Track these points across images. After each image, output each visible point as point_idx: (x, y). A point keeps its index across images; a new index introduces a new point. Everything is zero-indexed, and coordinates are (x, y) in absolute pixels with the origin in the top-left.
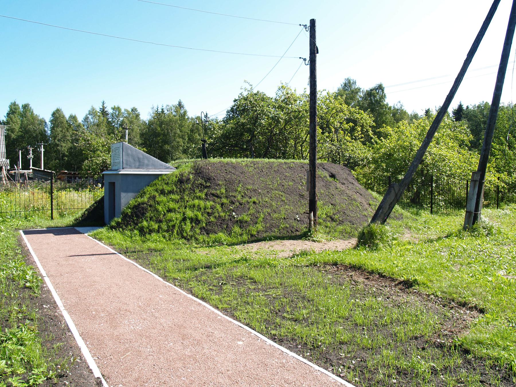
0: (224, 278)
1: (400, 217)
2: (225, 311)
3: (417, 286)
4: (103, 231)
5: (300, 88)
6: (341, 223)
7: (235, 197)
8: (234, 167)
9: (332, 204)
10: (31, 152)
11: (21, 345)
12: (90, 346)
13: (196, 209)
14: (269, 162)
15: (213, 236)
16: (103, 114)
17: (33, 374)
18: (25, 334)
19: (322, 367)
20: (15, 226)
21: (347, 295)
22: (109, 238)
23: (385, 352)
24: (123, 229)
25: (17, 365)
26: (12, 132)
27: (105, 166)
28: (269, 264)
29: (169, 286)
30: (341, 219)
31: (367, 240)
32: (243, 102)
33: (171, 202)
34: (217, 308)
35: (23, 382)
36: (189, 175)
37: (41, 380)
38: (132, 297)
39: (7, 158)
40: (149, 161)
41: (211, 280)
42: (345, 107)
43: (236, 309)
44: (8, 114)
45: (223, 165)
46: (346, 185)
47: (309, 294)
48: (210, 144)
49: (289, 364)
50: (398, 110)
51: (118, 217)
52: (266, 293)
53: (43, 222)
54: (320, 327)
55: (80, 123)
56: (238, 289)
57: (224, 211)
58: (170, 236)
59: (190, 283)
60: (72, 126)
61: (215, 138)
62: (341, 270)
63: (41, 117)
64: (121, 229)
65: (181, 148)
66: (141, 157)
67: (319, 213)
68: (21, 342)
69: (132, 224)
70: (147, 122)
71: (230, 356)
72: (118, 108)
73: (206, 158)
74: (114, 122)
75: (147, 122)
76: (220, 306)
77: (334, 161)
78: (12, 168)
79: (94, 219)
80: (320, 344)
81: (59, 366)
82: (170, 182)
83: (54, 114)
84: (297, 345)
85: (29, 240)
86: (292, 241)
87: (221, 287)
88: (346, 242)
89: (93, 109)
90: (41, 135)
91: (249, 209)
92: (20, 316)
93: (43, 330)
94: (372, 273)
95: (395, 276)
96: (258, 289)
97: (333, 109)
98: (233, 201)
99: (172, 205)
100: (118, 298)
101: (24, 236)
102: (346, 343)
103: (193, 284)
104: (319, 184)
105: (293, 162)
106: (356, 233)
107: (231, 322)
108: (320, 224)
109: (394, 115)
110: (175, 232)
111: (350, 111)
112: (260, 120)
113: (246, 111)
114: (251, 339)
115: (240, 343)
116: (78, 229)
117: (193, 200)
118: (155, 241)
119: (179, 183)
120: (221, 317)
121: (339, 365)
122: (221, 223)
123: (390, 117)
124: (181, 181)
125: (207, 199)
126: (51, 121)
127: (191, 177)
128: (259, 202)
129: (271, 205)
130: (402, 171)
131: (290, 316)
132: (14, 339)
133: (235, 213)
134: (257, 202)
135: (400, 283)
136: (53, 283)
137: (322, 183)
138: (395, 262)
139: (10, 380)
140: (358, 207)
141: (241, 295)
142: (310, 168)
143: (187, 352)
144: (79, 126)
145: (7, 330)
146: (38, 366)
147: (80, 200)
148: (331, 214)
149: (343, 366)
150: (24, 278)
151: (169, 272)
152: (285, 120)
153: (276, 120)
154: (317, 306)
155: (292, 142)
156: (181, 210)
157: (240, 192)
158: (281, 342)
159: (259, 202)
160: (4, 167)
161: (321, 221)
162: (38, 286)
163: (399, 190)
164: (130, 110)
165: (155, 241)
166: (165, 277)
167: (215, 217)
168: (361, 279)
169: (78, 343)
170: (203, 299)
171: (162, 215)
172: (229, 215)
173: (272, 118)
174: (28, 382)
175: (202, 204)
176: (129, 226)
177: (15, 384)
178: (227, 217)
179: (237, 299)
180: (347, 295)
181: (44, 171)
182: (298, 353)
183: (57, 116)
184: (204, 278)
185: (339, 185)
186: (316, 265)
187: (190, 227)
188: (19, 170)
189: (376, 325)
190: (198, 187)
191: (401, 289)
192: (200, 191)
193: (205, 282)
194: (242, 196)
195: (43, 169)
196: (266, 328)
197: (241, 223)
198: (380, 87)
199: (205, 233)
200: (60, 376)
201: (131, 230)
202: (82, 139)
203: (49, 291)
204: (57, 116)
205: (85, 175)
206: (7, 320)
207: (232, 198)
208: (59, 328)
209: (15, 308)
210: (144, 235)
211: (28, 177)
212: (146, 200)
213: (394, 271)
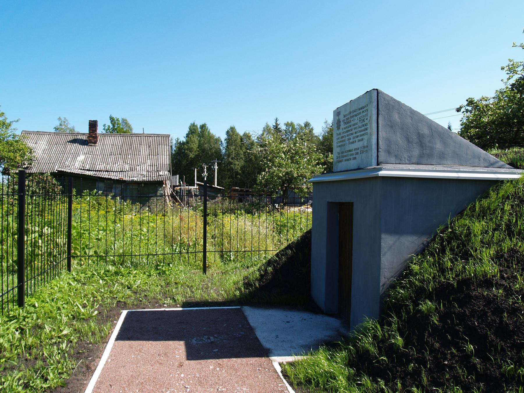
10: (205, 170)
40: (445, 144)
44: (188, 136)
55: (253, 141)
63: (217, 136)
70: (321, 138)
72: (292, 123)
75: (321, 138)
83: (228, 132)
89: (267, 126)
90: (216, 153)
144: (252, 144)
183: (231, 133)
204: (231, 133)
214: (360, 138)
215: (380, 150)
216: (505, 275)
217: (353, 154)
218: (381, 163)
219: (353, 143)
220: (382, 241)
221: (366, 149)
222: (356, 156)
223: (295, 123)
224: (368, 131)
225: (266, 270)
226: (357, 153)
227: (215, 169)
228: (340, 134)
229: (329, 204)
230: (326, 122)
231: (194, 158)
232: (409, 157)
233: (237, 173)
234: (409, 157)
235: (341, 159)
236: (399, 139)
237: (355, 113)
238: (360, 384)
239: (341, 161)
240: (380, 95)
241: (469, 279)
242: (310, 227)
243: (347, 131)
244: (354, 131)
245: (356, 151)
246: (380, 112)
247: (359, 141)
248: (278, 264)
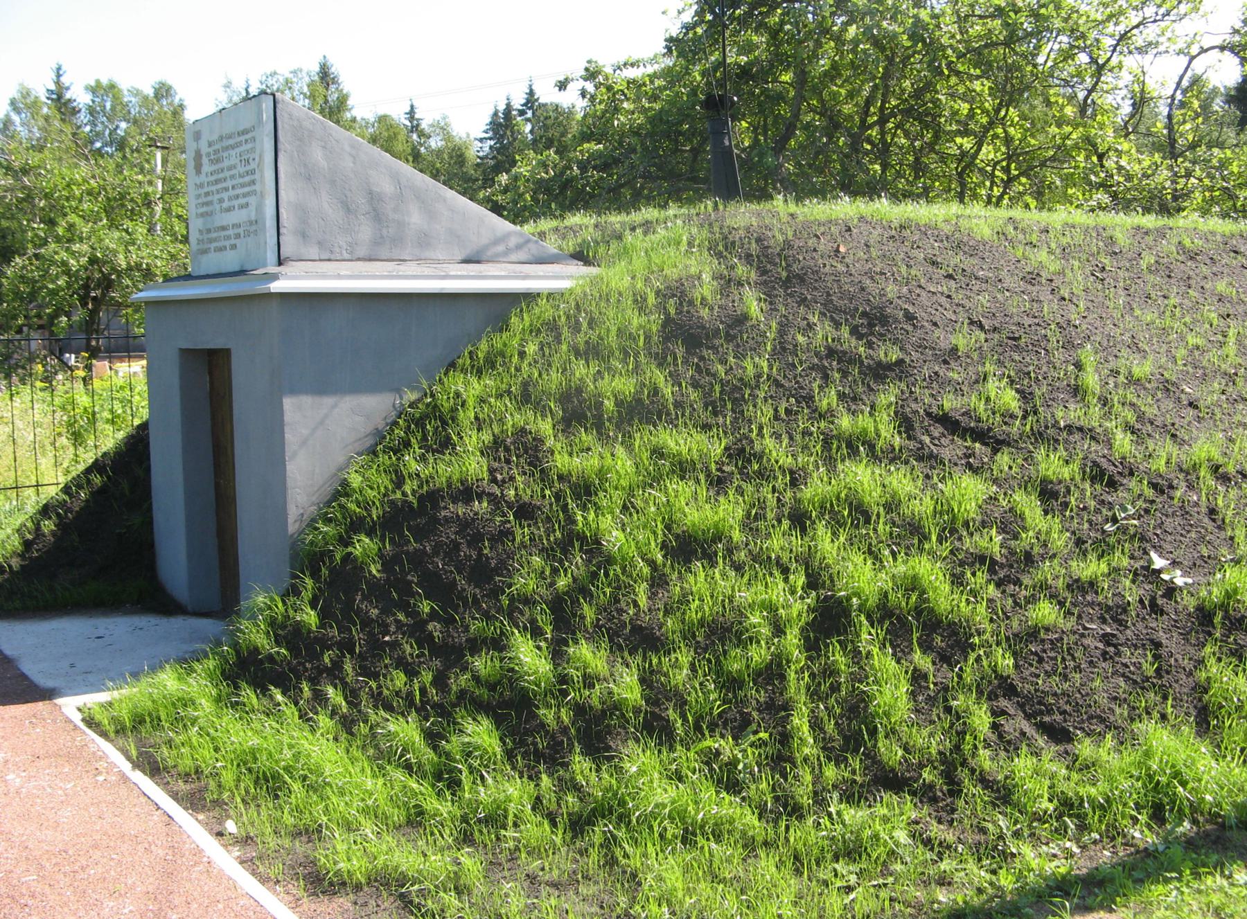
66: (386, 187)
72: (112, 86)
89: (26, 94)
99: (697, 509)
124: (685, 333)
164: (150, 92)
210: (554, 757)
214: (242, 201)
215: (282, 230)
216: (499, 477)
217: (229, 238)
218: (288, 259)
219: (229, 210)
220: (287, 429)
221: (254, 228)
222: (237, 242)
223: (124, 85)
224: (257, 187)
225: (38, 528)
226: (238, 236)
228: (201, 186)
229: (187, 354)
230: (227, 86)
232: (350, 244)
234: (350, 244)
235: (206, 246)
236: (326, 206)
237: (231, 142)
238: (237, 703)
239: (205, 252)
240: (279, 106)
241: (439, 490)
242: (144, 414)
243: (217, 182)
244: (229, 184)
245: (236, 231)
246: (280, 146)
247: (242, 207)
248: (69, 510)
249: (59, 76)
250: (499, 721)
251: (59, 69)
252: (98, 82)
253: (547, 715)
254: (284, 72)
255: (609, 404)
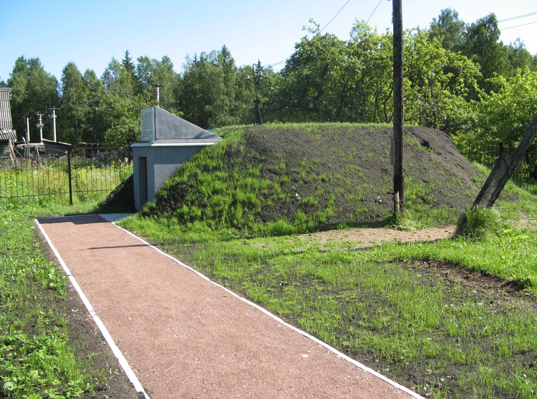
0: (285, 277)
1: (514, 198)
2: (286, 317)
3: (529, 288)
4: (133, 218)
5: (383, 27)
6: (436, 205)
7: (298, 173)
8: (297, 134)
9: (424, 181)
10: (41, 119)
11: (52, 354)
12: (129, 357)
13: (249, 189)
14: (341, 127)
15: (271, 225)
16: (127, 68)
17: (70, 386)
18: (55, 342)
19: (403, 385)
20: (28, 214)
21: (439, 299)
22: (141, 227)
23: (482, 369)
24: (158, 217)
25: (51, 375)
26: (18, 95)
27: (132, 137)
28: (341, 260)
29: (217, 287)
30: (436, 200)
31: (469, 227)
32: (307, 48)
33: (217, 182)
34: (277, 314)
35: (59, 395)
36: (238, 146)
37: (79, 392)
38: (173, 300)
39: (13, 129)
41: (269, 280)
42: (442, 51)
43: (300, 316)
45: (282, 132)
46: (443, 156)
47: (391, 296)
48: (266, 103)
49: (364, 380)
50: (516, 50)
51: (152, 201)
52: (337, 296)
53: (60, 208)
54: (403, 337)
55: (98, 81)
56: (303, 291)
57: (284, 192)
58: (217, 224)
59: (243, 284)
60: (89, 85)
61: (271, 96)
62: (434, 266)
64: (156, 217)
65: (227, 108)
67: (406, 193)
68: (51, 351)
69: (169, 209)
71: (293, 370)
73: (260, 123)
74: (141, 77)
75: (182, 76)
76: (281, 312)
77: (429, 124)
78: (20, 141)
79: (122, 203)
80: (402, 358)
81: (96, 379)
82: (215, 155)
83: (66, 71)
84: (374, 359)
85: (46, 231)
86: (371, 230)
87: (281, 288)
88: (442, 230)
89: (114, 62)
91: (316, 188)
92: (47, 321)
93: (73, 339)
94: (473, 270)
95: (502, 275)
96: (328, 291)
97: (426, 54)
98: (296, 178)
99: (218, 185)
100: (157, 301)
101: (40, 226)
102: (435, 357)
103: (246, 284)
104: (406, 155)
105: (374, 127)
106: (456, 219)
107: (293, 331)
108: (408, 207)
109: (510, 58)
110: (223, 218)
111: (449, 57)
112: (331, 71)
113: (312, 58)
114: (318, 351)
115: (305, 356)
116: (103, 216)
117: (245, 178)
118: (198, 231)
119: (226, 157)
120: (282, 324)
121: (423, 382)
122: (281, 207)
123: (504, 60)
124: (229, 154)
125: (262, 177)
126: (63, 80)
127: (242, 148)
128: (330, 180)
129: (345, 184)
130: (519, 136)
131: (367, 324)
132: (44, 347)
133: (299, 194)
134: (327, 180)
135: (508, 284)
136: (80, 283)
137: (411, 154)
138: (503, 257)
139: (46, 391)
140: (458, 184)
141: (306, 297)
142: (394, 132)
143: (242, 366)
144: (98, 84)
145: (35, 337)
146: (74, 378)
147: (103, 179)
148: (423, 194)
149: (429, 384)
150: (47, 278)
151: (216, 269)
152: (363, 69)
153: (351, 70)
154: (400, 313)
155: (372, 99)
156: (229, 191)
157: (304, 166)
158: (354, 354)
159: (330, 180)
160: (10, 141)
161: (409, 203)
162: (63, 286)
163: (512, 163)
165: (199, 231)
166: (212, 277)
167: (273, 200)
168: (459, 279)
169: (114, 353)
170: (259, 303)
171: (206, 199)
172: (291, 197)
173: (347, 69)
174: (64, 394)
175: (256, 183)
176: (166, 213)
177: (52, 396)
178: (288, 200)
179: (301, 304)
180: (439, 299)
181: (57, 144)
182: (376, 368)
183: (70, 72)
184: (260, 277)
185: (433, 156)
186: (402, 261)
187: (241, 213)
188: (27, 143)
189: (474, 336)
190: (250, 161)
191: (508, 292)
192: (253, 166)
193: (261, 282)
194: (308, 172)
195: (55, 141)
196: (336, 338)
197: (306, 207)
198: (491, 20)
199: (260, 220)
200: (99, 389)
201: (169, 218)
202: (104, 102)
203: (76, 293)
204: (70, 72)
205: (108, 147)
206: (34, 326)
207: (294, 174)
208: (92, 336)
209: (41, 312)
210: (185, 224)
211: (39, 152)
212: (185, 178)
213: (501, 268)
223: (150, 58)
227: (53, 118)
230: (187, 57)
231: (23, 104)
233: (80, 122)
249: (127, 55)
250: (178, 218)
251: (127, 52)
252: (141, 57)
253: (186, 217)
254: (208, 52)
255: (211, 168)
